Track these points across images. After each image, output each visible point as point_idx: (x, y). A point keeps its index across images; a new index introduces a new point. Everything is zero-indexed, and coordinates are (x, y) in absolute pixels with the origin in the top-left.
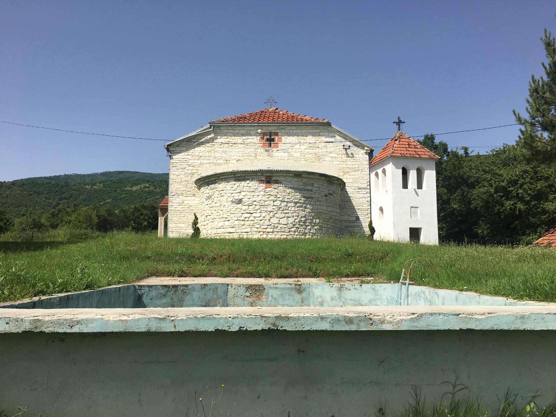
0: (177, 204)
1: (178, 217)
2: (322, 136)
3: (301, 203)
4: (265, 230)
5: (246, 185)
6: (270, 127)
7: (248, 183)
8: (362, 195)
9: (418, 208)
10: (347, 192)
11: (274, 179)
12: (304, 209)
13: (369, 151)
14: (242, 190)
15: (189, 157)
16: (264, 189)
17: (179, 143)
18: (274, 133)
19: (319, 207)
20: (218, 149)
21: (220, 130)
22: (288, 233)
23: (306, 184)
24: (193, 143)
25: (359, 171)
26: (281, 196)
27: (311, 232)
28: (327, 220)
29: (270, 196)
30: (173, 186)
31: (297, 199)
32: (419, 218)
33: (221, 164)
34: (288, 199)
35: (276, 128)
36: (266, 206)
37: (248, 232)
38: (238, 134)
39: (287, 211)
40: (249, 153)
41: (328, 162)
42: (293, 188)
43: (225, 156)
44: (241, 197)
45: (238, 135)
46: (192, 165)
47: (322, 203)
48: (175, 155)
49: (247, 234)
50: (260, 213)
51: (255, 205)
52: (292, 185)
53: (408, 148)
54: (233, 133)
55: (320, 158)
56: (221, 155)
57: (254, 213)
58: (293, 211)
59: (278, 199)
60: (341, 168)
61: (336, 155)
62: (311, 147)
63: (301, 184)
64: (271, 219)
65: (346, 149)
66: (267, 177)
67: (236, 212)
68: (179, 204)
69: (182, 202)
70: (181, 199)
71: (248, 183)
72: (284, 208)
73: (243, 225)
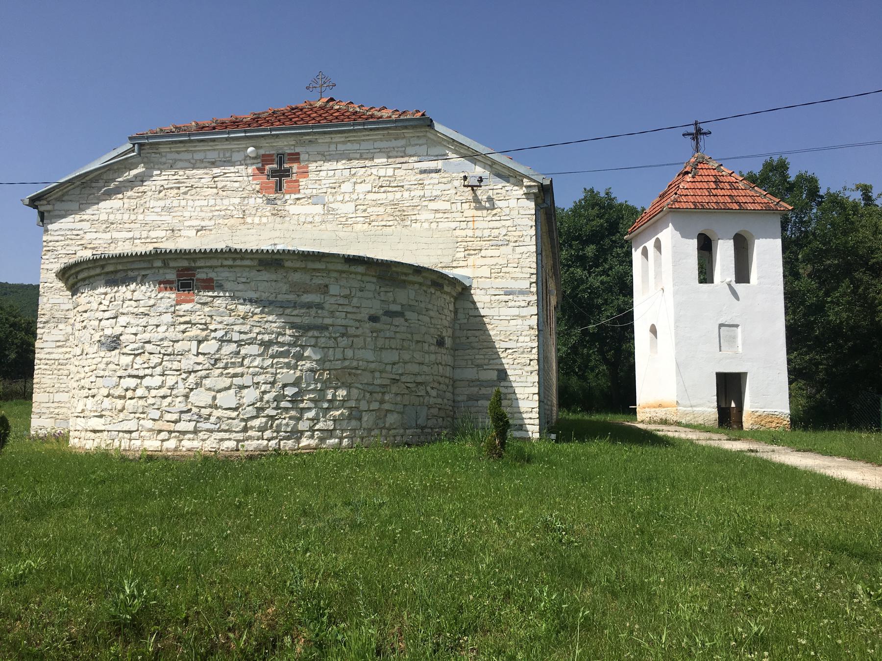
0: (54, 345)
1: (54, 376)
2: (411, 156)
3: (282, 344)
4: (172, 427)
5: (128, 295)
6: (277, 140)
7: (134, 291)
8: (515, 311)
9: (737, 326)
10: (474, 303)
11: (201, 275)
12: (293, 362)
13: (535, 190)
14: (121, 311)
15: (86, 226)
16: (171, 306)
17: (60, 193)
18: (289, 154)
19: (349, 353)
20: (152, 203)
21: (158, 155)
22: (242, 434)
23: (299, 289)
24: (94, 191)
25: (507, 245)
26: (220, 326)
27: (317, 427)
28: (378, 389)
29: (190, 326)
30: (45, 300)
31: (268, 334)
32: (740, 350)
33: (160, 240)
34: (241, 333)
35: (293, 143)
36: (178, 355)
37: (130, 432)
38: (202, 161)
39: (239, 370)
40: (226, 209)
41: (426, 225)
42: (256, 302)
43: (168, 218)
44: (118, 330)
45: (203, 165)
46: (92, 246)
47: (359, 342)
48: (52, 223)
49: (127, 436)
50: (160, 375)
51: (151, 354)
52: (256, 291)
53: (714, 189)
54: (188, 161)
55: (406, 213)
56: (159, 218)
57: (147, 375)
58: (257, 369)
59: (213, 335)
60: (460, 240)
61: (447, 205)
62: (382, 187)
63: (285, 288)
64: (192, 393)
65: (472, 187)
66: (181, 272)
67: (106, 373)
68: (58, 344)
69: (63, 339)
70: (63, 332)
71: (134, 291)
72: (229, 360)
73: (121, 411)
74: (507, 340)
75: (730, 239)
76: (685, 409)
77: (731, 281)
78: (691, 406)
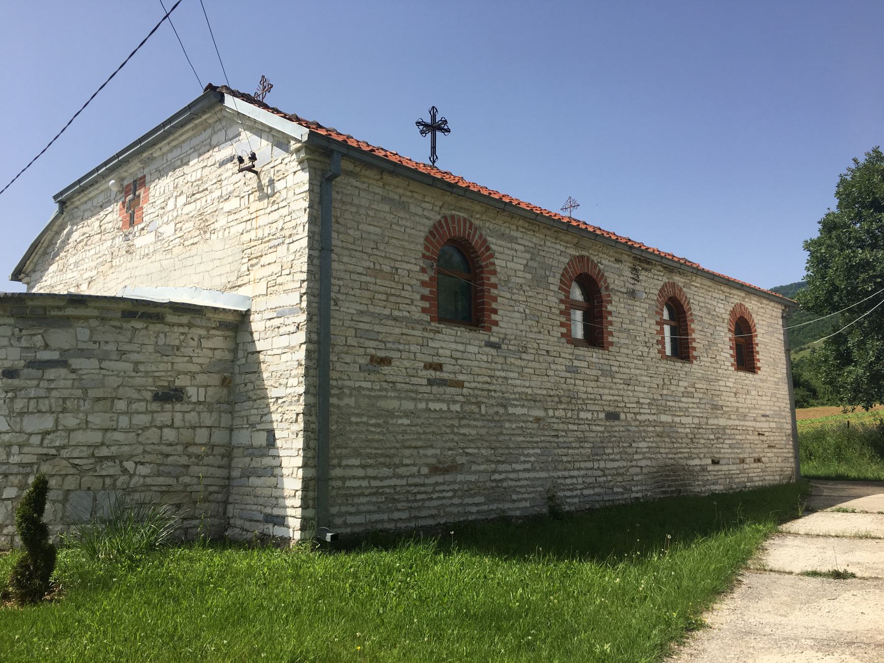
74: (277, 385)
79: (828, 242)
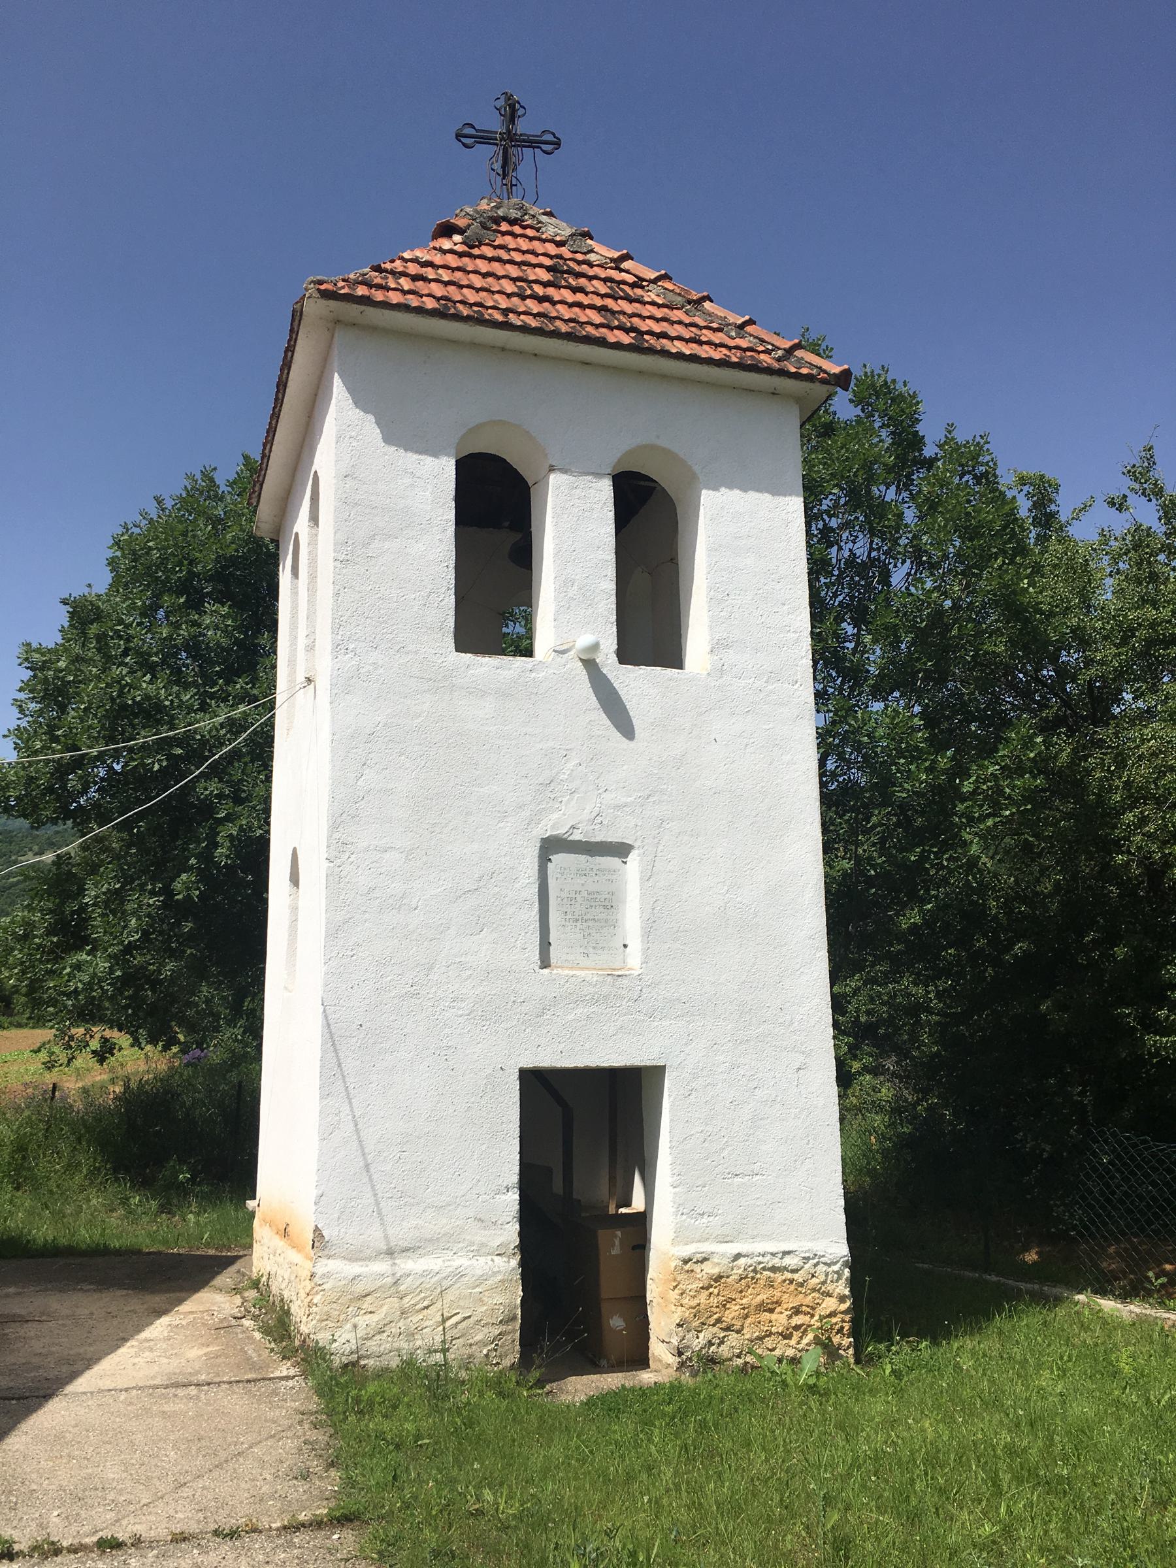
9: (621, 850)
32: (634, 959)
75: (598, 475)
76: (355, 1269)
77: (595, 647)
78: (390, 1253)
79: (77, 649)
